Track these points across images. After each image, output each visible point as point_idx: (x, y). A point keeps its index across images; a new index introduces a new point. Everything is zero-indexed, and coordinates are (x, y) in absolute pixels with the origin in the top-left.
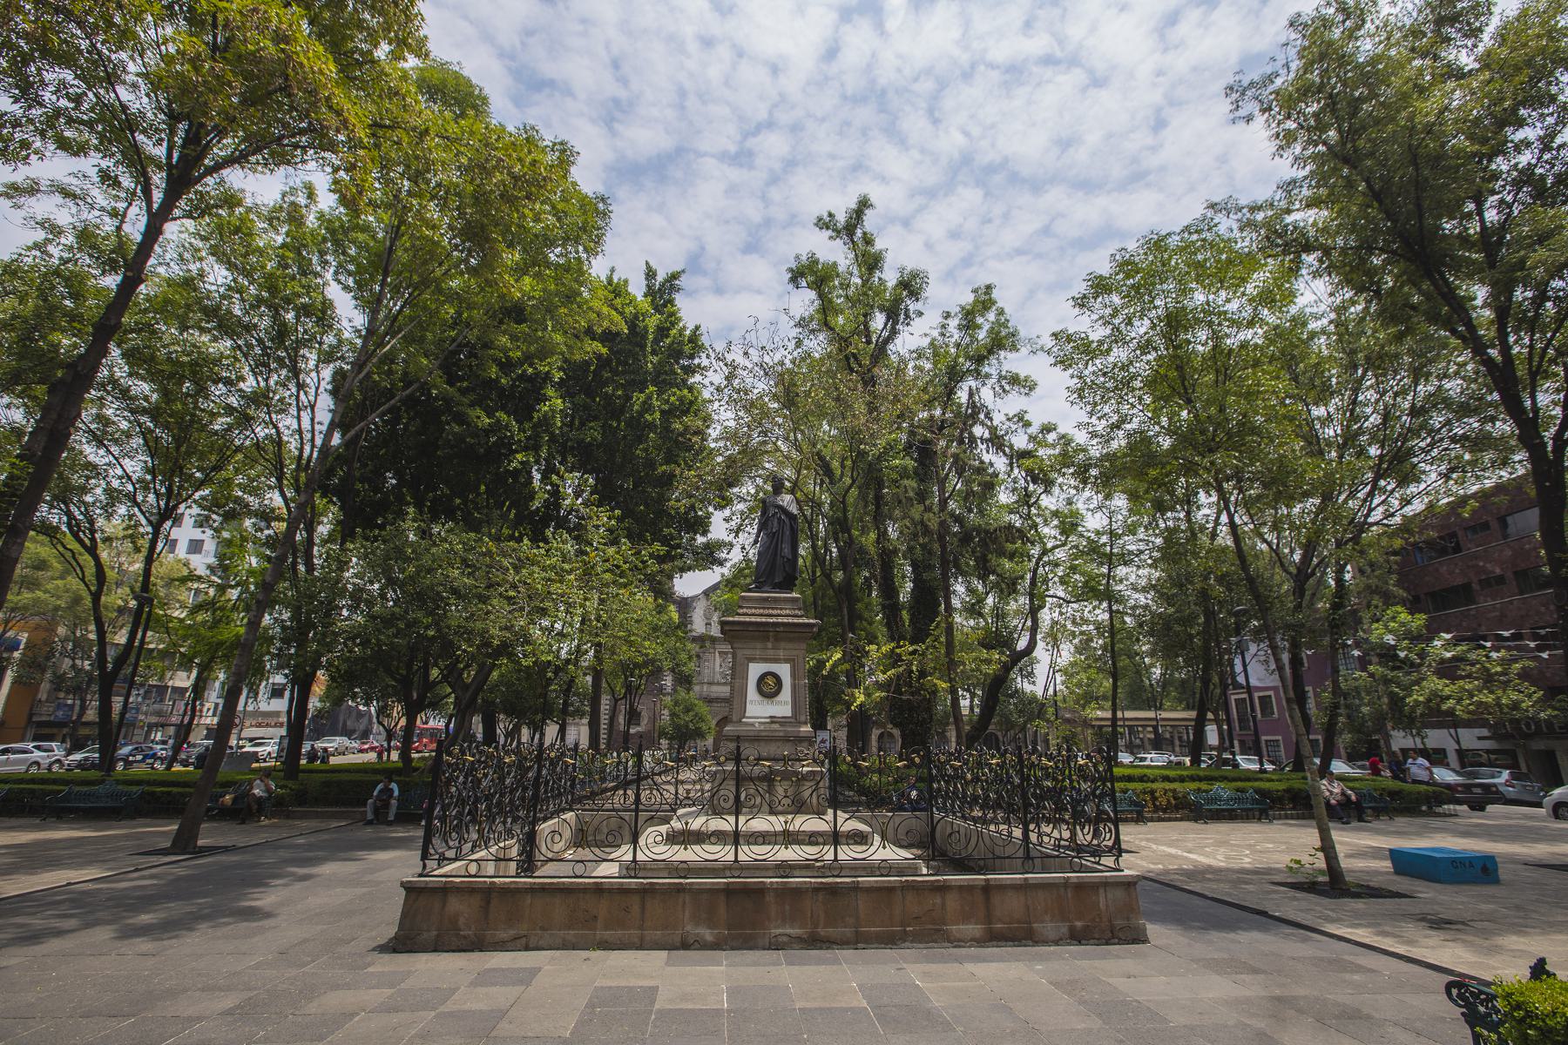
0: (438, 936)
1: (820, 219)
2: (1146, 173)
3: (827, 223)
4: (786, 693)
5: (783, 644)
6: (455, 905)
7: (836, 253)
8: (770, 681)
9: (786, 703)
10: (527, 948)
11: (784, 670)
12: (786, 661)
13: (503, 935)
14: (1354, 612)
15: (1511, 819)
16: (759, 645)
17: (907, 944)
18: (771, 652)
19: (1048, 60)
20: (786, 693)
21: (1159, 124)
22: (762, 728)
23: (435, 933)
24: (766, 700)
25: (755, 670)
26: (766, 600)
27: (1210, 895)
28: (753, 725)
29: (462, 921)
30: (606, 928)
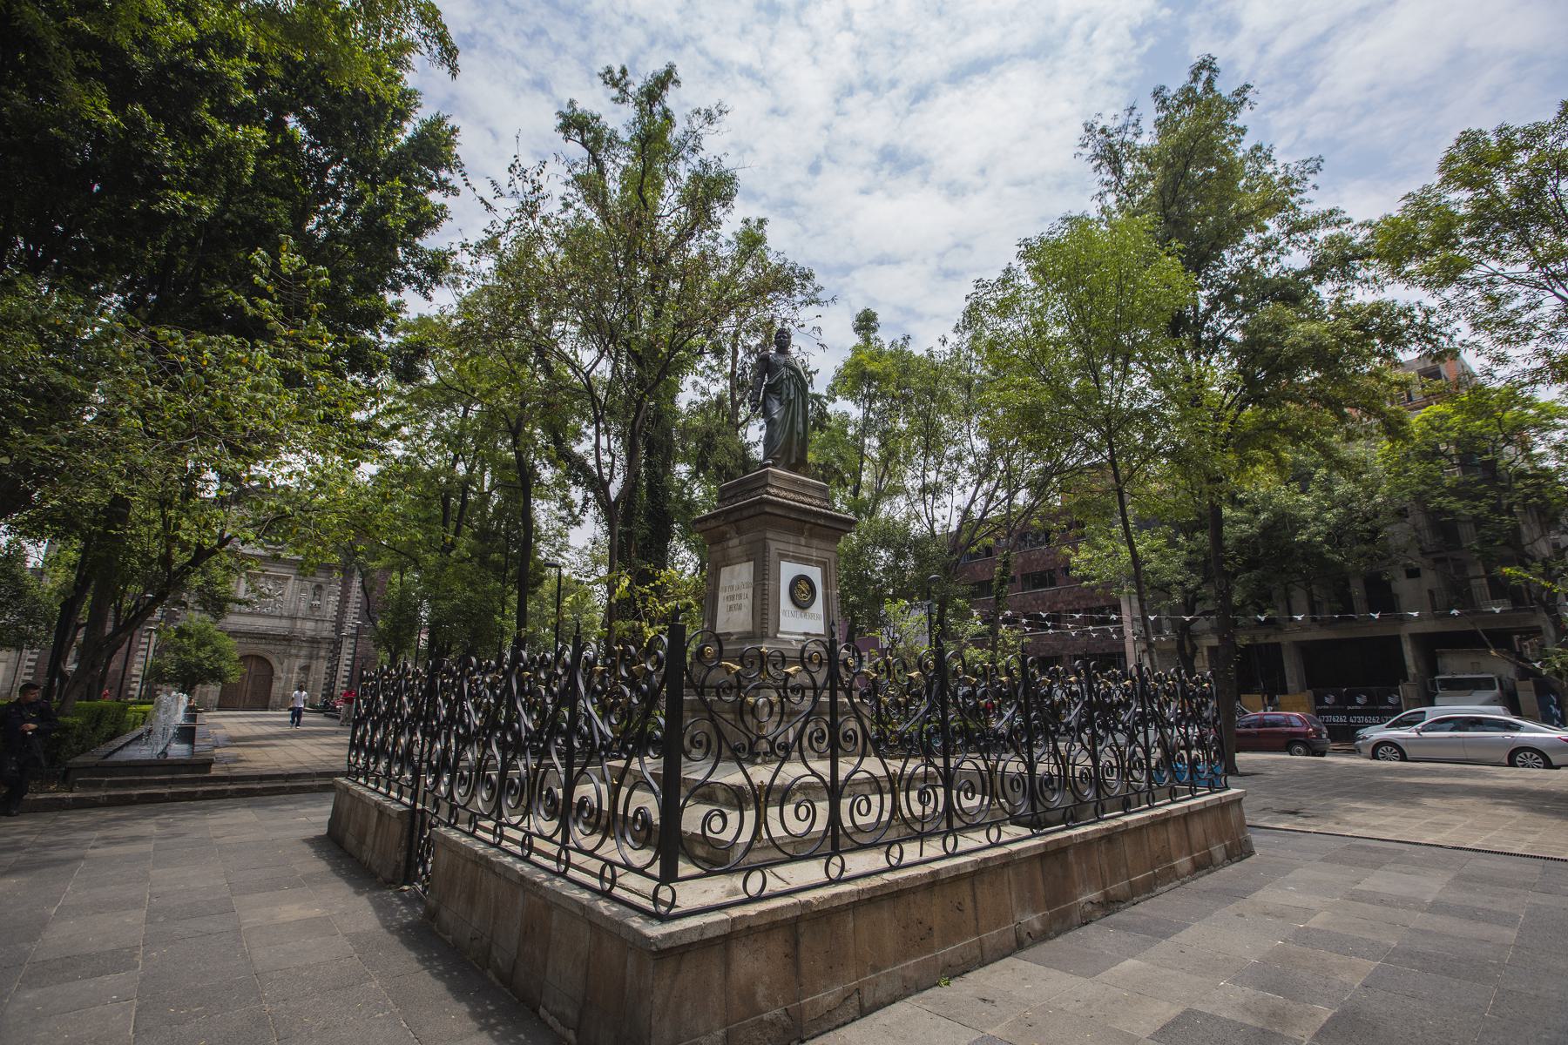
0: (727, 1036)
1: (609, 71)
2: (794, 203)
3: (615, 80)
4: (818, 607)
5: (815, 542)
6: (748, 963)
7: (619, 119)
8: (803, 586)
9: (819, 618)
10: (864, 1012)
11: (815, 574)
12: (818, 563)
13: (827, 996)
14: (464, 602)
15: (264, 789)
16: (792, 539)
17: (1159, 890)
18: (804, 550)
19: (748, 72)
20: (818, 607)
21: (815, 169)
23: (720, 1033)
24: (799, 612)
25: (788, 571)
26: (795, 481)
27: (1467, 801)
28: (789, 642)
29: (761, 991)
30: (945, 944)
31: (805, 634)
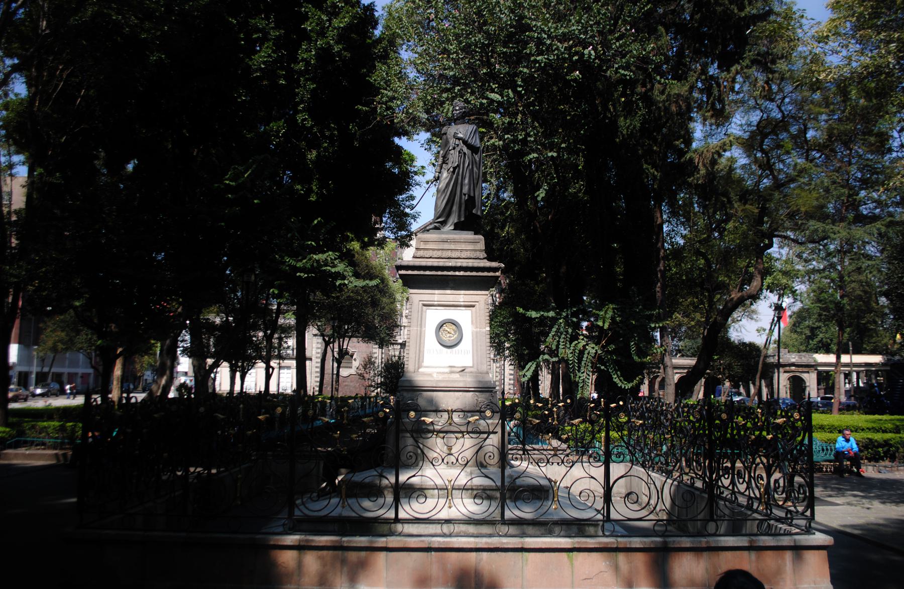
22: (440, 377)
28: (430, 375)
31: (451, 367)
